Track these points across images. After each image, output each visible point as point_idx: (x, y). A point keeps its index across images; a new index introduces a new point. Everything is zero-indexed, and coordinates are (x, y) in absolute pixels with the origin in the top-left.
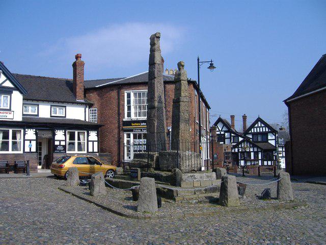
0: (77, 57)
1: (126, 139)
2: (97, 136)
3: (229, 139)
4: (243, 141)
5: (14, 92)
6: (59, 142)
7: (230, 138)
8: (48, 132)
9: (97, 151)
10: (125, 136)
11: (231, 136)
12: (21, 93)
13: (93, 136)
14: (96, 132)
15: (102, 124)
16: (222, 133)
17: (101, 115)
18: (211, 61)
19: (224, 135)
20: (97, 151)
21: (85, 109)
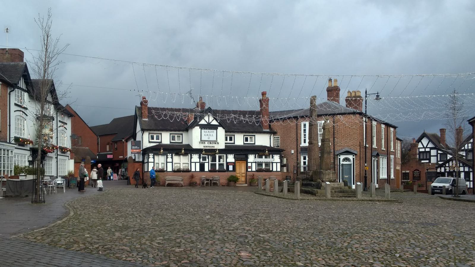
0: (264, 94)
1: (302, 160)
2: (234, 158)
3: (436, 157)
4: (451, 160)
5: (219, 128)
6: (251, 163)
7: (437, 156)
8: (109, 149)
9: (280, 170)
10: (302, 158)
11: (437, 153)
12: (224, 128)
13: (277, 158)
14: (279, 155)
15: (284, 148)
16: (428, 150)
17: (283, 140)
18: (378, 93)
19: (430, 152)
20: (280, 170)
21: (270, 137)
